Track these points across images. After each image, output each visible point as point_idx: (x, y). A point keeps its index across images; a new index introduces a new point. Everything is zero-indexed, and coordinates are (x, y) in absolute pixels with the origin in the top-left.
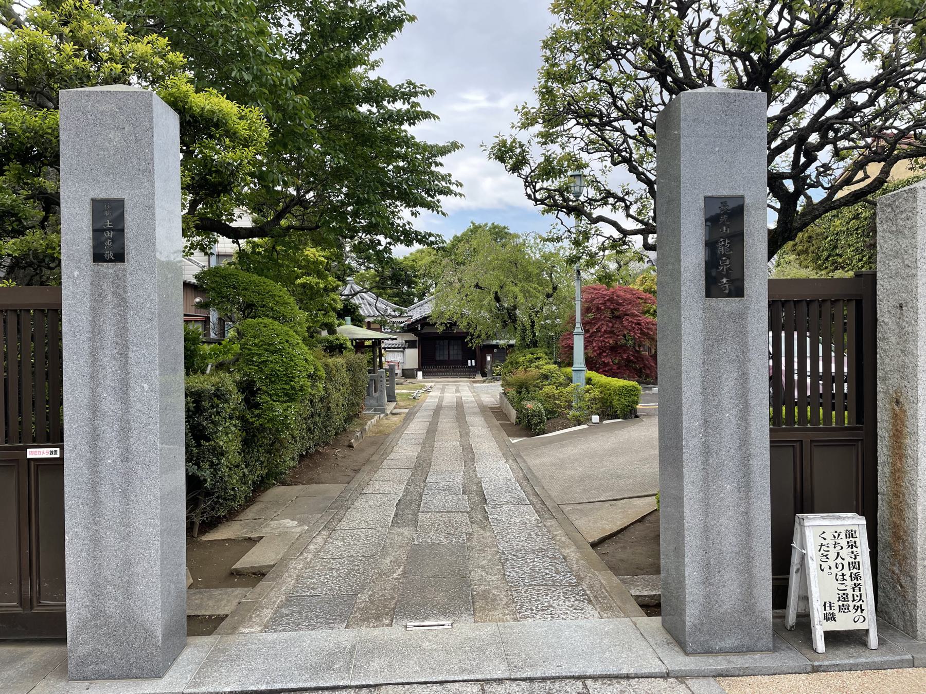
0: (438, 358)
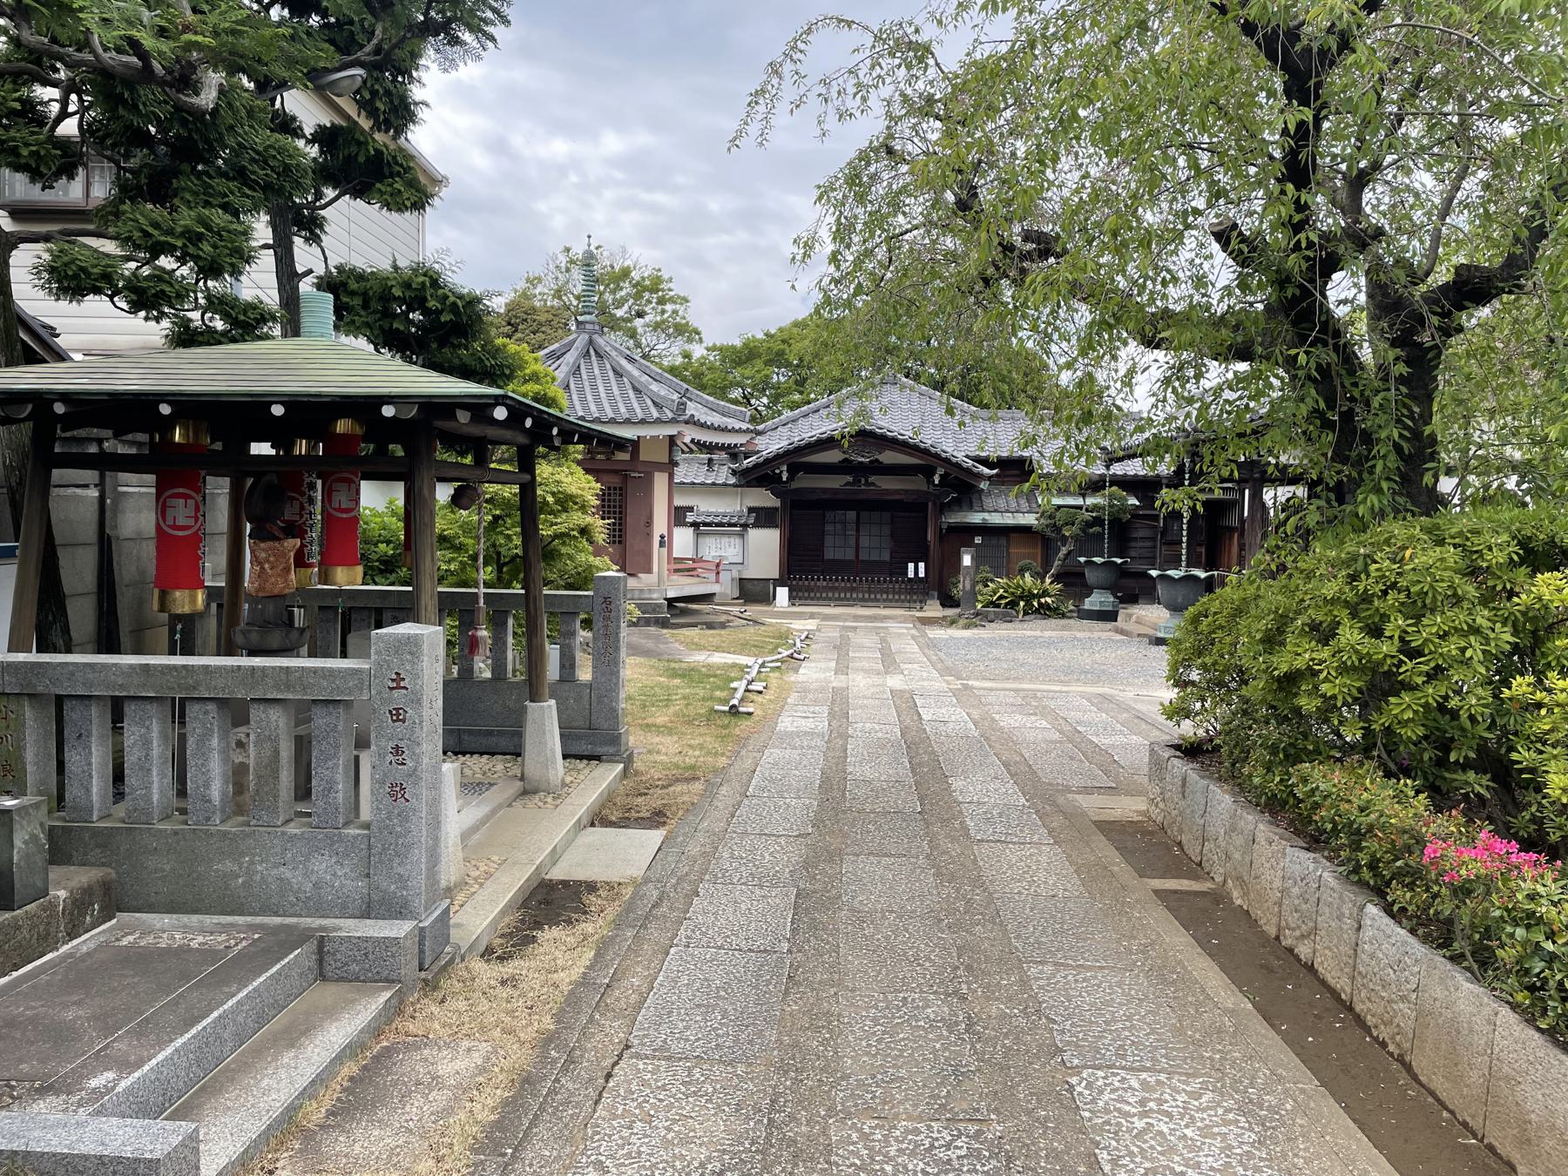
0: (829, 554)
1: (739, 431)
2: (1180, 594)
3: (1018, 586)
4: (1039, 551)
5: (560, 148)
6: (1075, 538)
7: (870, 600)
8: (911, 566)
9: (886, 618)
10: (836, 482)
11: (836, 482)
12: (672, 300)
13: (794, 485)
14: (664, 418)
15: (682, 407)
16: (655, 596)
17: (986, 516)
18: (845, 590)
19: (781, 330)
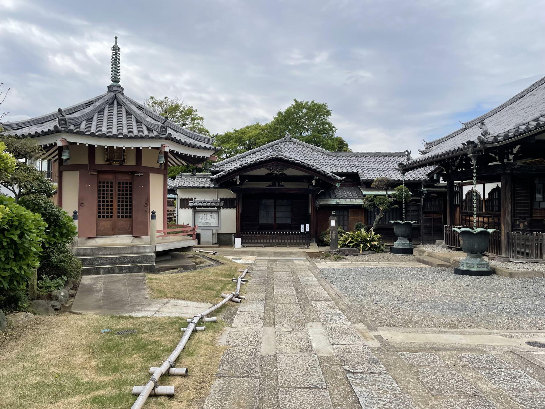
0: (261, 221)
1: (205, 148)
2: (476, 244)
3: (359, 236)
4: (363, 218)
5: (168, 77)
6: (385, 211)
7: (282, 243)
8: (302, 226)
9: (291, 254)
10: (264, 185)
11: (264, 185)
12: (197, 119)
13: (244, 187)
14: (151, 136)
15: (164, 129)
16: (148, 250)
17: (338, 201)
18: (270, 238)
19: (241, 129)
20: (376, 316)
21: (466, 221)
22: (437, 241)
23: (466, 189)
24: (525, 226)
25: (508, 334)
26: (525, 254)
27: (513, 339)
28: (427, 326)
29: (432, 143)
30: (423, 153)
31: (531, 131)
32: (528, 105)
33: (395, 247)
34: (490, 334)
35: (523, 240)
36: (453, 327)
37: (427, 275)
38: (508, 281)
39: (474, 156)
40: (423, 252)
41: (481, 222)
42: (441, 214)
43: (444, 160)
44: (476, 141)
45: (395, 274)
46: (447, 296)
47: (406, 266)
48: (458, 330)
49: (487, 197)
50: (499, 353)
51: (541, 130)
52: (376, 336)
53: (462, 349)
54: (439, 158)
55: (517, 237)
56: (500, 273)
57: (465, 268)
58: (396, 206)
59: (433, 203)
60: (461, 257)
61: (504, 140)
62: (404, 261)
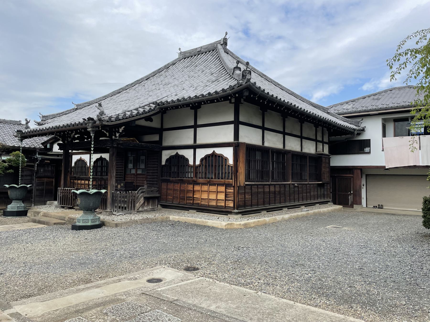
2: (91, 202)
20: (5, 289)
21: (74, 183)
22: (48, 202)
23: (75, 158)
24: (121, 187)
25: (132, 277)
26: (124, 208)
27: (137, 280)
28: (63, 288)
29: (47, 116)
30: (39, 124)
31: (133, 117)
32: (125, 99)
33: (8, 210)
34: (120, 281)
35: (123, 197)
36: (87, 283)
37: (48, 234)
38: (115, 230)
39: (93, 131)
40: (38, 213)
41: (86, 184)
42: (53, 178)
43: (60, 132)
44: (95, 118)
45: (15, 238)
46: (71, 252)
47: (22, 228)
48: (93, 284)
49: (198, 162)
50: (135, 298)
51: (139, 117)
52: (11, 315)
53: (104, 304)
54: (60, 129)
55: (119, 195)
56: (108, 225)
57: (81, 224)
58: (11, 171)
59: (46, 169)
60: (77, 215)
61: (116, 121)
62: (19, 223)
